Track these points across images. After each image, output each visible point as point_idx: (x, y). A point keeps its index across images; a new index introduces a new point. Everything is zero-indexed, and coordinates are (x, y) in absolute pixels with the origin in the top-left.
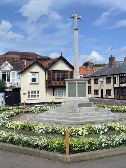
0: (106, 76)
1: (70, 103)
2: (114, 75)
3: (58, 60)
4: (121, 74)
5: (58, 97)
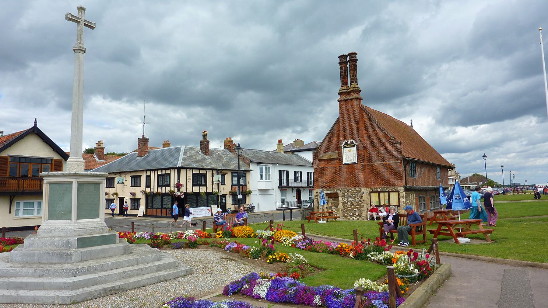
0: (130, 172)
1: (55, 237)
2: (147, 171)
4: (162, 170)
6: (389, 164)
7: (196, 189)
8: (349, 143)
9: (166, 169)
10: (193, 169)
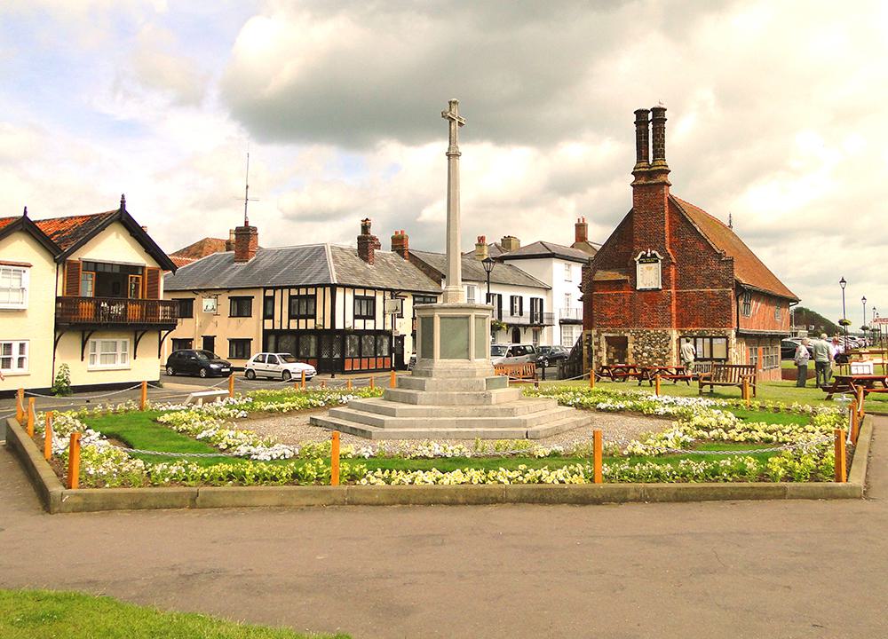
0: (229, 290)
3: (108, 225)
4: (298, 288)
5: (98, 365)
6: (713, 293)
7: (359, 325)
8: (649, 255)
9: (307, 287)
10: (354, 287)
